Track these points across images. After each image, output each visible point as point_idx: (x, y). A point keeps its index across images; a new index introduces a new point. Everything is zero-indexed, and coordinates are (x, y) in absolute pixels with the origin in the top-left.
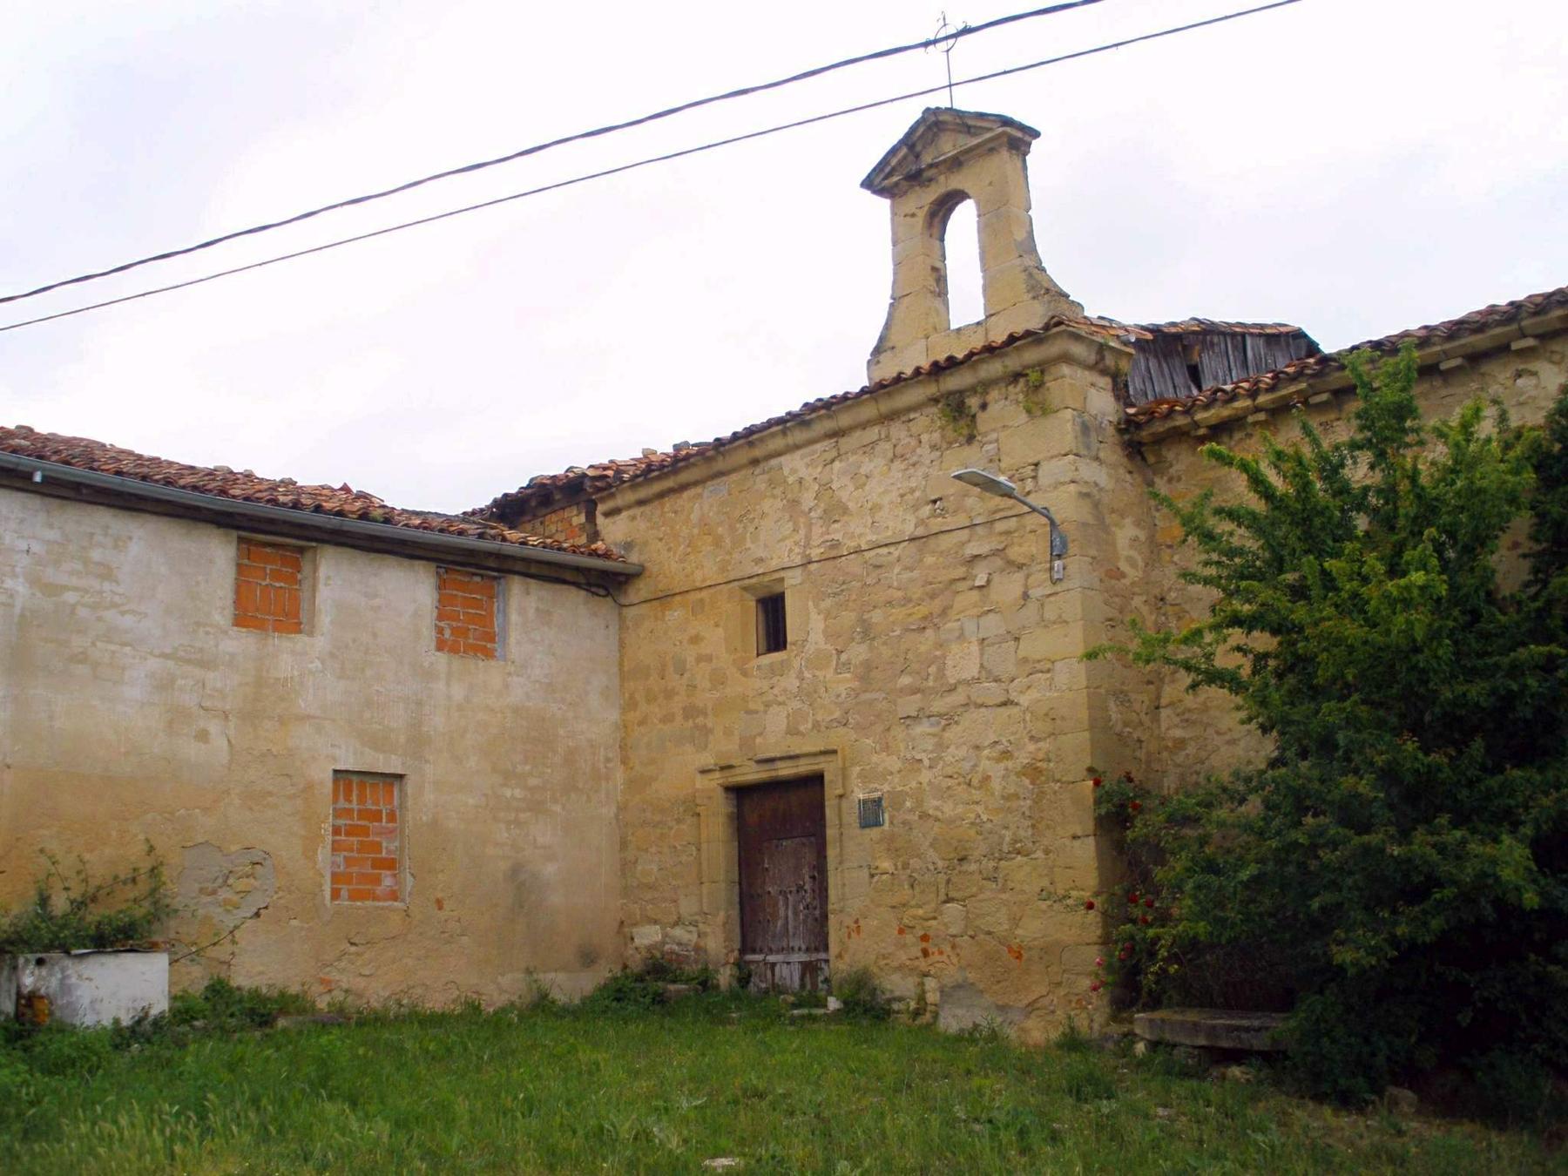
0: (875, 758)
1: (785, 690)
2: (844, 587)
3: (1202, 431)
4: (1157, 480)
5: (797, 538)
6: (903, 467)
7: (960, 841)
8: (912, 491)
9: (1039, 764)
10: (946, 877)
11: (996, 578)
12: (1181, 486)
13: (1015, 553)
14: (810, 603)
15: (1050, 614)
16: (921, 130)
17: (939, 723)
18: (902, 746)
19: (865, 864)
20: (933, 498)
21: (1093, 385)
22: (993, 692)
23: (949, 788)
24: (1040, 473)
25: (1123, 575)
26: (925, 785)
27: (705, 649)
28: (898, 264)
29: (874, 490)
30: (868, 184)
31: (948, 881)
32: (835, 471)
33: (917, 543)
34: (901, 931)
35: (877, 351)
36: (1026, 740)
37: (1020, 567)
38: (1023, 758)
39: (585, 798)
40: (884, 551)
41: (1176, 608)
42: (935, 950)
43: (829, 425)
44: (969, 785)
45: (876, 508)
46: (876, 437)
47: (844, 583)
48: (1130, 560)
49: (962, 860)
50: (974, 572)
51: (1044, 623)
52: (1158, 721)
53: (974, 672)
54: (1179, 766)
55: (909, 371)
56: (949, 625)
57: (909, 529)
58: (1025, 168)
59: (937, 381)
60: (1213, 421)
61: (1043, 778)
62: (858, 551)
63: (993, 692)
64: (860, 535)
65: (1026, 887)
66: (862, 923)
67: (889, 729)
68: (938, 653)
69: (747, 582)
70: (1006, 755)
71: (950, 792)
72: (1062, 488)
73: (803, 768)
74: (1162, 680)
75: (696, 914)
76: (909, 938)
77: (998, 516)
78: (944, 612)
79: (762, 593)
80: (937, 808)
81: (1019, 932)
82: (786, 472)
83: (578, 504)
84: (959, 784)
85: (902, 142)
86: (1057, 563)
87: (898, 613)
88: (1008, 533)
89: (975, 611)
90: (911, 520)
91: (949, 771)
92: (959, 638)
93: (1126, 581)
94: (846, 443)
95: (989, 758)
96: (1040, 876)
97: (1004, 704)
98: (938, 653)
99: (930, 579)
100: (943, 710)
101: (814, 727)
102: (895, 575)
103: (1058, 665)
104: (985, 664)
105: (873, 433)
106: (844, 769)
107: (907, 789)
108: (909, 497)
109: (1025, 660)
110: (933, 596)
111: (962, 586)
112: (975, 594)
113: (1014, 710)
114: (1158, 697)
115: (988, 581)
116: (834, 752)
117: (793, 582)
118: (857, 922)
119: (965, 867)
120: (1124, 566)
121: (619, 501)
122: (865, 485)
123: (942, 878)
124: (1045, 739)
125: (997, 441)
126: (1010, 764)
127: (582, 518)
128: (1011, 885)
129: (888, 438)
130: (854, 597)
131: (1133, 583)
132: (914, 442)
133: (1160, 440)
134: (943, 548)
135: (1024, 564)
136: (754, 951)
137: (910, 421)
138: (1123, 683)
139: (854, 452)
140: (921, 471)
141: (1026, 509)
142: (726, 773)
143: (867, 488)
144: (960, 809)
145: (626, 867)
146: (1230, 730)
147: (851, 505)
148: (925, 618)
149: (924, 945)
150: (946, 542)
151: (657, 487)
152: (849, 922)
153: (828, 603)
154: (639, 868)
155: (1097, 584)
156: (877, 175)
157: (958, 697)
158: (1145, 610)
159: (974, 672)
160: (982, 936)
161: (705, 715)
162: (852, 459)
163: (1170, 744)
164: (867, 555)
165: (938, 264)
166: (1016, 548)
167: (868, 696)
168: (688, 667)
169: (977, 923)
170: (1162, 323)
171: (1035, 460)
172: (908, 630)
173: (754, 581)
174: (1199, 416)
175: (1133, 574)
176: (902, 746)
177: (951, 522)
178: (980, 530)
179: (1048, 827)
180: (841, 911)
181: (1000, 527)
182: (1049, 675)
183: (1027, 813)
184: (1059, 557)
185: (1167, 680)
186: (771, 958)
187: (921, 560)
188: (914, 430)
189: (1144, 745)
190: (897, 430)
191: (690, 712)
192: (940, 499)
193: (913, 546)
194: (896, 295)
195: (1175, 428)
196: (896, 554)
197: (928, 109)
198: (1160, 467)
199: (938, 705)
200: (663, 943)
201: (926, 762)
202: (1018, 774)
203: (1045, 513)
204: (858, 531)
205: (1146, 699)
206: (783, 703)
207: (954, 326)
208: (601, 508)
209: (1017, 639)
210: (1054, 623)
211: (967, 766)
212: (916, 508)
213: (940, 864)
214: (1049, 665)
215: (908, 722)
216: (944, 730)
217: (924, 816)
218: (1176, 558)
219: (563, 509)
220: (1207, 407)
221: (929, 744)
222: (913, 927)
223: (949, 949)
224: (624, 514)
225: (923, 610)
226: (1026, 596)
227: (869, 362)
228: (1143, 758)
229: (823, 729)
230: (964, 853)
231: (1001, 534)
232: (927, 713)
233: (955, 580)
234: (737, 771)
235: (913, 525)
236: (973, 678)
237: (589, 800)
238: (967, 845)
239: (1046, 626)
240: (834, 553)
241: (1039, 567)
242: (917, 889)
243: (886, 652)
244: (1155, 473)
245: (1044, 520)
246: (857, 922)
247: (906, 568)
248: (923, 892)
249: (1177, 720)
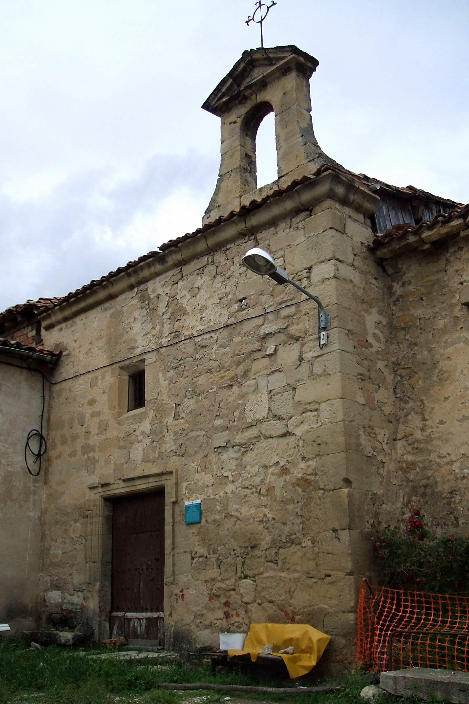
0: (197, 476)
1: (143, 432)
2: (182, 362)
3: (427, 247)
4: (395, 285)
5: (154, 332)
6: (221, 280)
7: (252, 534)
8: (227, 295)
9: (309, 477)
10: (242, 560)
11: (281, 348)
12: (411, 288)
13: (294, 330)
14: (160, 374)
15: (318, 369)
16: (242, 65)
17: (240, 450)
18: (215, 467)
19: (188, 550)
20: (240, 298)
21: (350, 217)
22: (278, 427)
23: (246, 496)
24: (312, 275)
25: (371, 346)
26: (229, 494)
27: (97, 408)
28: (223, 154)
29: (203, 295)
30: (207, 106)
31: (243, 563)
32: (179, 288)
33: (230, 329)
34: (211, 599)
35: (208, 212)
36: (300, 460)
37: (297, 339)
38: (297, 472)
39: (17, 505)
40: (208, 335)
41: (408, 371)
42: (234, 613)
43: (178, 257)
44: (259, 493)
45: (203, 308)
46: (205, 263)
47: (181, 360)
48: (375, 335)
49: (254, 547)
50: (266, 345)
51: (312, 376)
52: (395, 449)
53: (264, 413)
54: (411, 481)
55: (226, 215)
56: (248, 382)
57: (224, 320)
58: (308, 86)
59: (245, 221)
60: (435, 238)
61: (311, 488)
62: (192, 337)
63: (278, 427)
64: (193, 327)
65: (299, 568)
66: (185, 592)
67: (206, 456)
68: (240, 402)
69: (123, 363)
70: (285, 471)
71: (246, 499)
72: (327, 282)
73: (151, 484)
74: (398, 421)
75: (83, 583)
76: (217, 604)
77: (283, 306)
78: (246, 373)
79: (133, 370)
80: (237, 510)
81: (293, 601)
82: (150, 291)
83: (32, 324)
84: (252, 493)
85: (229, 75)
86: (323, 333)
87: (215, 376)
88: (289, 317)
89: (268, 371)
90: (226, 313)
91: (247, 483)
92: (254, 391)
93: (373, 350)
94: (188, 269)
95: (273, 474)
96: (309, 559)
97: (284, 435)
98: (240, 402)
99: (237, 352)
100: (243, 441)
101: (159, 455)
102: (214, 351)
103: (323, 406)
104: (272, 408)
105: (204, 260)
106: (177, 484)
107: (217, 497)
108: (225, 299)
109: (300, 403)
110: (238, 364)
111: (257, 355)
112: (266, 361)
113: (292, 439)
114: (395, 432)
115: (276, 351)
116: (171, 473)
117: (149, 361)
118: (182, 591)
119: (257, 552)
120: (371, 340)
121: (53, 319)
122: (197, 294)
123: (239, 560)
124: (313, 459)
125: (283, 256)
126: (288, 478)
127: (34, 333)
128: (288, 566)
129: (213, 263)
130: (187, 368)
131: (377, 352)
132: (229, 263)
133: (397, 256)
134: (245, 330)
135: (300, 337)
136: (118, 610)
137: (228, 249)
138: (370, 420)
139: (192, 274)
140: (233, 281)
141: (304, 297)
142: (105, 489)
143: (198, 296)
144: (252, 511)
145: (43, 553)
146: (449, 454)
147: (188, 308)
148: (232, 379)
149: (226, 609)
150: (248, 326)
151: (75, 308)
152: (177, 591)
153: (172, 373)
154: (52, 552)
155: (352, 350)
156: (214, 99)
157: (252, 433)
158: (386, 371)
159: (262, 413)
160: (267, 604)
161: (94, 451)
162: (190, 278)
163: (404, 465)
164: (197, 339)
165: (251, 154)
166: (295, 327)
167: (194, 433)
168: (86, 420)
169: (263, 594)
170: (400, 187)
171: (308, 265)
172: (220, 388)
173: (128, 362)
174: (425, 234)
175: (377, 346)
176: (215, 467)
177: (252, 312)
178: (270, 316)
179: (315, 523)
180: (172, 584)
181: (285, 312)
182: (315, 413)
183: (300, 513)
184: (324, 329)
185: (401, 420)
186: (129, 615)
187: (231, 340)
188: (230, 256)
189: (386, 465)
190: (220, 258)
191: (87, 449)
192: (245, 298)
193: (225, 332)
194: (221, 174)
195: (408, 244)
196: (215, 337)
197: (246, 51)
198: (397, 276)
199: (240, 438)
200: (63, 603)
201: (231, 478)
202: (294, 485)
203: (316, 300)
204: (192, 325)
205: (387, 433)
206: (141, 441)
207: (259, 187)
208: (44, 324)
209: (294, 389)
210: (320, 376)
211: (258, 480)
212: (228, 306)
213: (238, 550)
214: (316, 406)
215: (219, 451)
216: (243, 455)
217: (228, 516)
218: (407, 337)
219: (24, 328)
220: (430, 227)
221: (233, 465)
222: (219, 596)
223: (243, 613)
224: (56, 328)
225: (232, 373)
226: (301, 359)
227: (203, 217)
228: (385, 474)
229: (165, 457)
230: (255, 543)
231: (285, 318)
232: (232, 444)
233: (253, 351)
234: (112, 487)
235: (227, 318)
236: (263, 418)
237: (21, 507)
238: (257, 536)
239: (314, 379)
240: (176, 340)
241: (311, 338)
242: (222, 569)
243: (206, 403)
244: (393, 281)
245: (316, 305)
246: (182, 591)
247: (221, 346)
248: (226, 570)
249: (409, 449)
